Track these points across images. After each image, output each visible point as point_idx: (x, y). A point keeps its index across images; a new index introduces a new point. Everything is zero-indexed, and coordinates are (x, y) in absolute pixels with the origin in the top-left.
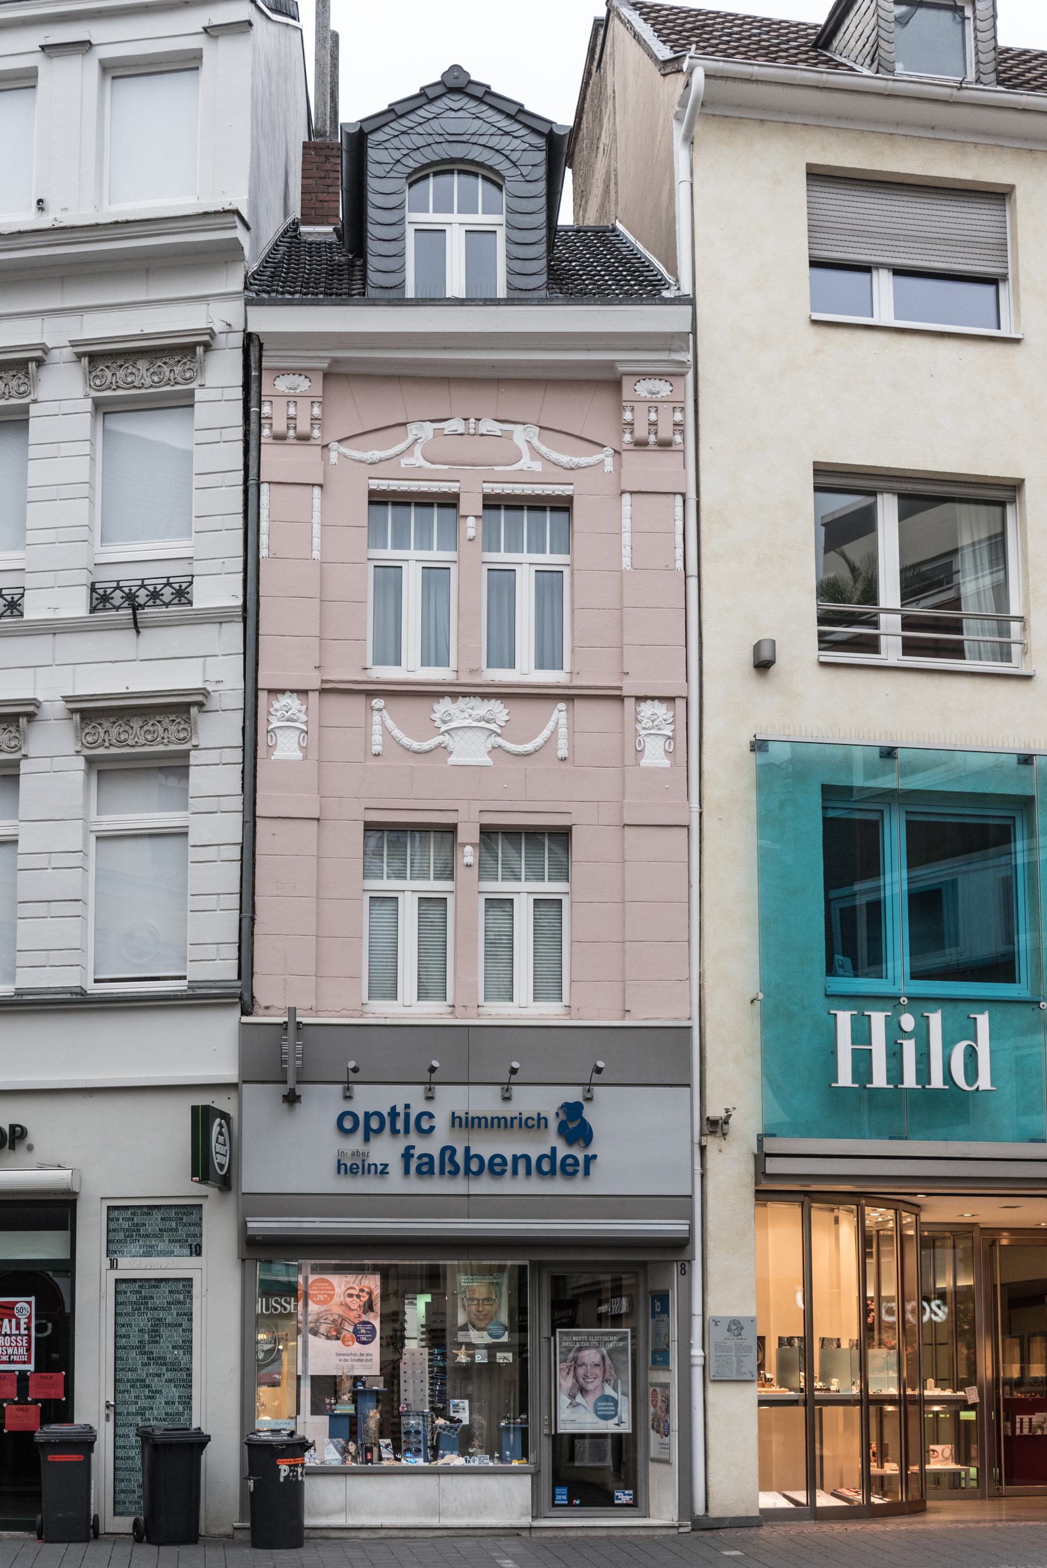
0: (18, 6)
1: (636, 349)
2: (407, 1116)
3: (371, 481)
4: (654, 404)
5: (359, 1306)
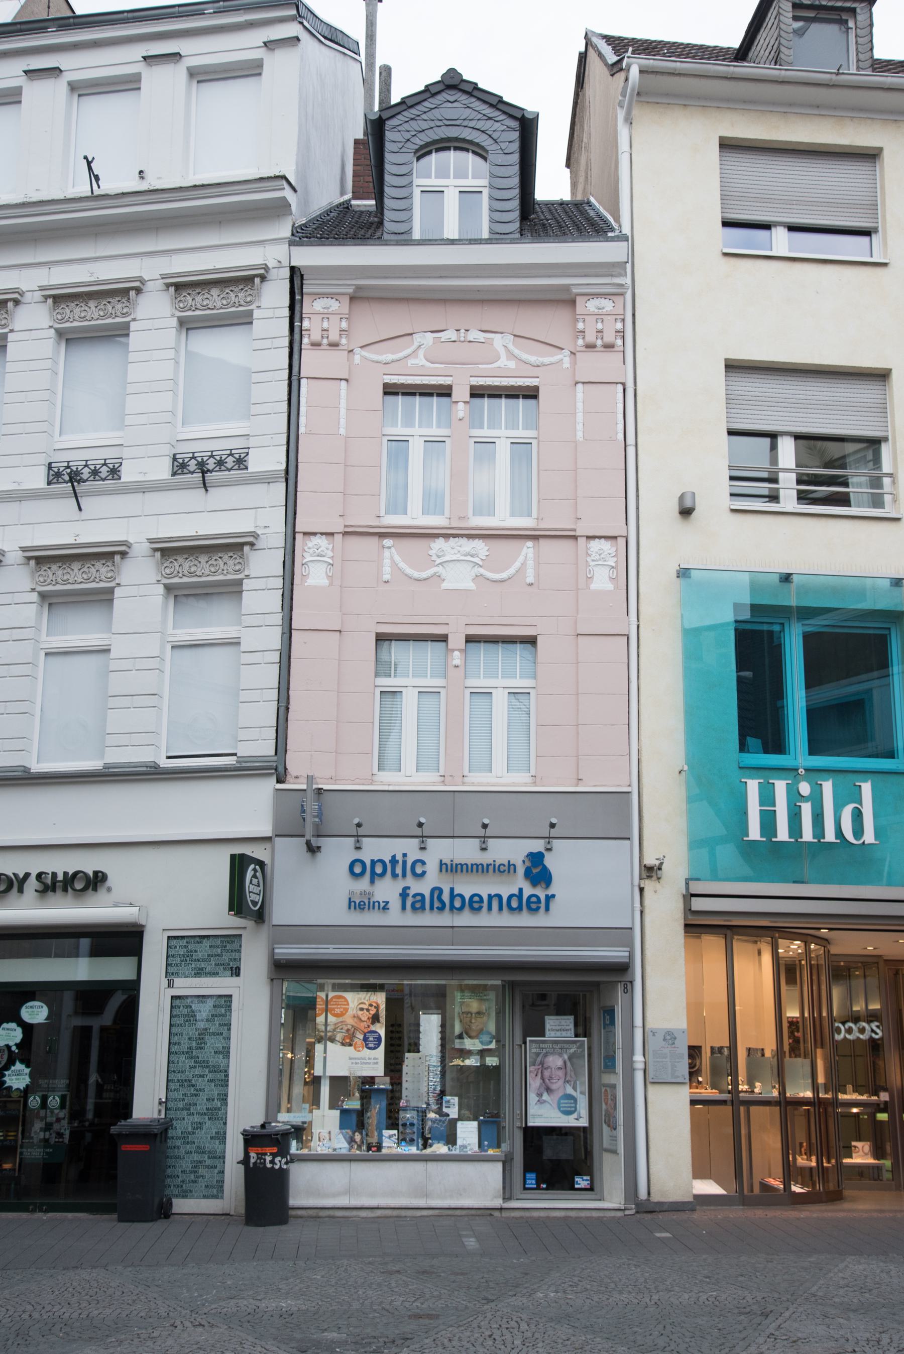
0: (125, 27)
1: (586, 276)
2: (404, 863)
3: (385, 377)
4: (600, 317)
5: (368, 1018)
